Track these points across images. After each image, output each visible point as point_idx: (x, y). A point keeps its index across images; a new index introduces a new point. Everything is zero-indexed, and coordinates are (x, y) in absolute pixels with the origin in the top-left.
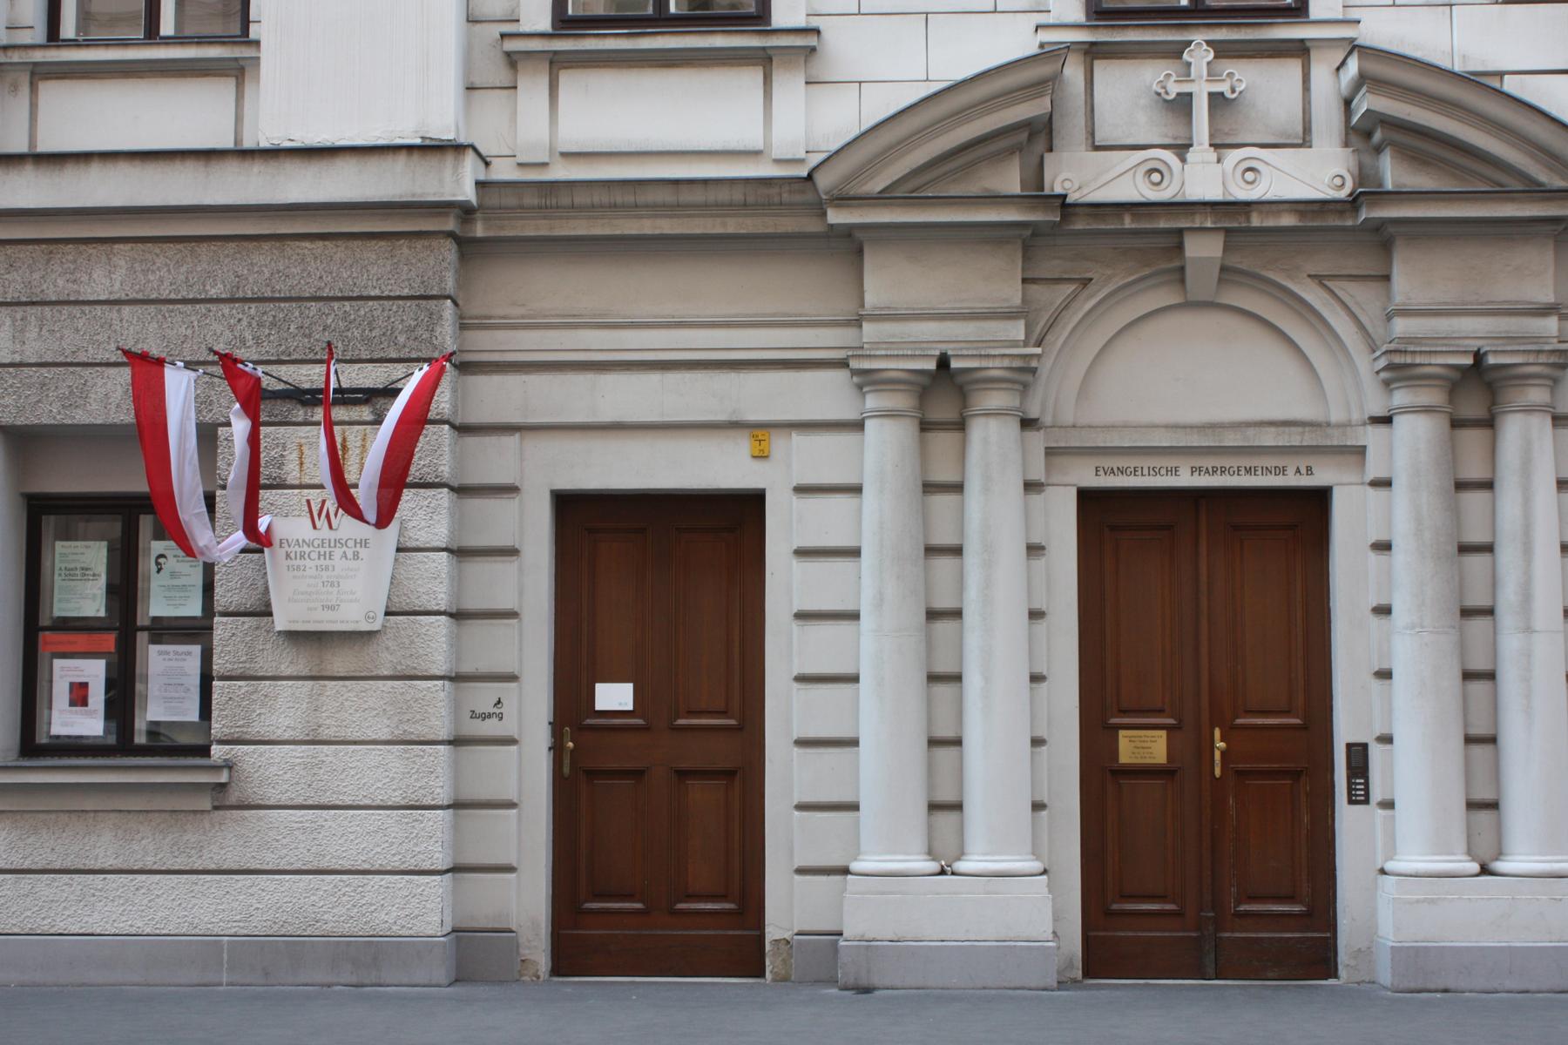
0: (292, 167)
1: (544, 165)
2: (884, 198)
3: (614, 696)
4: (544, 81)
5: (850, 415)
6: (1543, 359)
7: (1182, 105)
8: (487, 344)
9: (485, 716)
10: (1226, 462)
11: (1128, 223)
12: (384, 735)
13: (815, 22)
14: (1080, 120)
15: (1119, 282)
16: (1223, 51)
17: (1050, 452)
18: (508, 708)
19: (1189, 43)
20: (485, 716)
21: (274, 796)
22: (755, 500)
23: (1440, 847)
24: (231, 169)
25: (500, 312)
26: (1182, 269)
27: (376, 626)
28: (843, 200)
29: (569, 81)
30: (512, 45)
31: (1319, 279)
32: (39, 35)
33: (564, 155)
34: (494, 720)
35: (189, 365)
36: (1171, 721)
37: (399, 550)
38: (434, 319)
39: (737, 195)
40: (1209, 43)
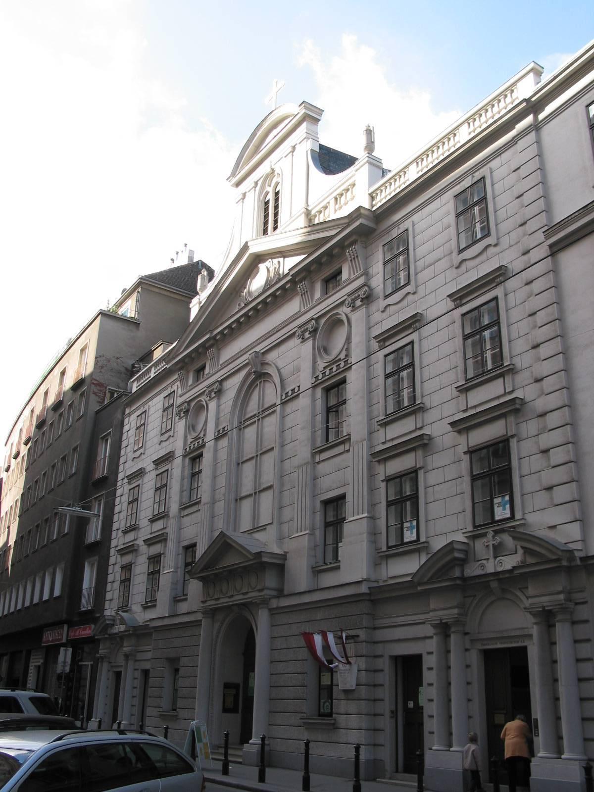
2: (430, 581)
8: (379, 623)
11: (477, 581)
16: (496, 532)
23: (546, 750)
24: (318, 593)
28: (420, 584)
29: (390, 561)
30: (380, 555)
31: (520, 589)
32: (321, 563)
35: (318, 634)
37: (358, 671)
40: (492, 531)
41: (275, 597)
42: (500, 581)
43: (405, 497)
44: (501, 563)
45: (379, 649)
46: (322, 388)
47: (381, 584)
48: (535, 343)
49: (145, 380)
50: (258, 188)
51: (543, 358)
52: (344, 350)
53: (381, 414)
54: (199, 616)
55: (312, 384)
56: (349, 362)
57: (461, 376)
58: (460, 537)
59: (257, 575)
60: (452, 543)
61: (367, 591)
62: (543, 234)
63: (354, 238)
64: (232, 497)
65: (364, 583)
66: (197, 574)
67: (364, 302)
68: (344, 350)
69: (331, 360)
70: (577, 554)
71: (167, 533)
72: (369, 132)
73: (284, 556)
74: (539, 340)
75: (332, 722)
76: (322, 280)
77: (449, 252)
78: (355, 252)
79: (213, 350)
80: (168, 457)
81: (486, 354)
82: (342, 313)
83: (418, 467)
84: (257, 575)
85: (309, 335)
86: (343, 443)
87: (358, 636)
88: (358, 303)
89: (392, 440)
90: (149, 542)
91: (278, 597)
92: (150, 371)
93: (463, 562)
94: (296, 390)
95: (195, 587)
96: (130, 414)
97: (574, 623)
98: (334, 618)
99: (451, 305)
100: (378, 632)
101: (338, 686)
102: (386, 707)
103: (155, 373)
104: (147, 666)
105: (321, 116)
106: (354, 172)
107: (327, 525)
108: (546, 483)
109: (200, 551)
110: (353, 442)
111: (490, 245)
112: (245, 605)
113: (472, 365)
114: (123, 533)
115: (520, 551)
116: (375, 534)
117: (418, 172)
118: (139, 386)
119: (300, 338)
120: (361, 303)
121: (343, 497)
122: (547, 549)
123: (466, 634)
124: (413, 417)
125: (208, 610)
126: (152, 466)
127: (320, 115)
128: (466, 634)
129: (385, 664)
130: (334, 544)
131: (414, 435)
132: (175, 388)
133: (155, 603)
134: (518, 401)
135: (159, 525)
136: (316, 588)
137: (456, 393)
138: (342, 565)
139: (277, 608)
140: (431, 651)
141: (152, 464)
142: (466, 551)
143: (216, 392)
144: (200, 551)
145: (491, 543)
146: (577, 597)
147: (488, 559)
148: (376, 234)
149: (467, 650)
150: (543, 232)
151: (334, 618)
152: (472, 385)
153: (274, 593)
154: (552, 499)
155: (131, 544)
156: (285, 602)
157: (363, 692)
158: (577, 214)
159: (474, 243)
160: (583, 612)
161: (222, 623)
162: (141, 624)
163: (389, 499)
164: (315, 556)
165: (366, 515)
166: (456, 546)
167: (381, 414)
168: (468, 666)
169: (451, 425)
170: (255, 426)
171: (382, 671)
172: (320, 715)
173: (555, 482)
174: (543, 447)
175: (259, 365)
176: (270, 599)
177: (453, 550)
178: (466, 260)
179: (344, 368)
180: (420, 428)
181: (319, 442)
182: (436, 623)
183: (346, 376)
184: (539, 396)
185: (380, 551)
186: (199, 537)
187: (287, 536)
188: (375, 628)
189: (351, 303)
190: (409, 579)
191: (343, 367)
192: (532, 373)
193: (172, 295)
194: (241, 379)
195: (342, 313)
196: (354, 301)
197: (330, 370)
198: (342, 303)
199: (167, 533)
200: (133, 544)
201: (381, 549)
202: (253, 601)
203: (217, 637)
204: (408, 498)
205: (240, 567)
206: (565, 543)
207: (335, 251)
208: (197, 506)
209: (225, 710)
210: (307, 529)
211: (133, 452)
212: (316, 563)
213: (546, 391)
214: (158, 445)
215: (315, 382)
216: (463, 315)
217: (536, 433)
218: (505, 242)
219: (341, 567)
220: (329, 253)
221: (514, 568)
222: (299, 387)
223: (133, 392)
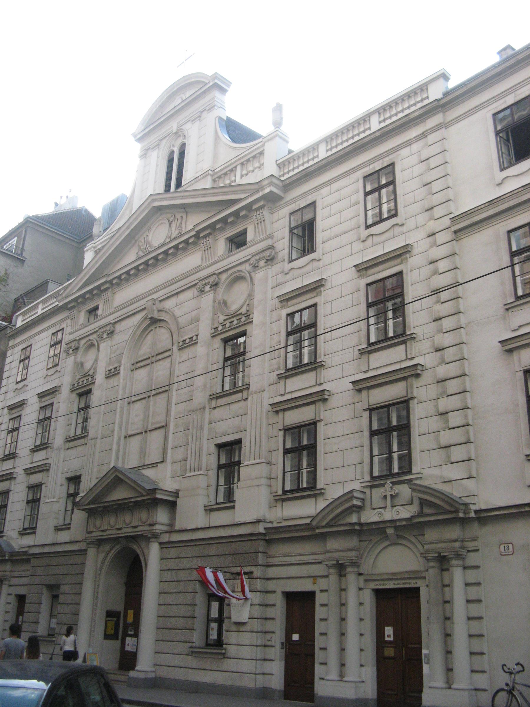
0: (290, 521)
1: (281, 522)
2: (327, 526)
3: (296, 637)
4: (281, 504)
5: (326, 574)
6: (453, 553)
7: (385, 497)
9: (269, 641)
10: (399, 582)
11: (374, 527)
13: (325, 487)
14: (369, 503)
15: (376, 540)
16: (393, 483)
17: (366, 581)
18: (273, 640)
19: (386, 483)
20: (269, 641)
21: (231, 656)
22: (312, 594)
25: (275, 554)
26: (388, 536)
27: (246, 621)
28: (318, 527)
33: (285, 520)
36: (395, 645)
38: (257, 557)
39: (305, 527)
41: (167, 532)
42: (396, 528)
43: (234, 462)
44: (398, 512)
45: (271, 585)
47: (275, 525)
48: (437, 316)
49: (30, 317)
51: (444, 331)
52: (93, 368)
53: (281, 368)
55: (211, 334)
56: (251, 317)
57: (282, 367)
58: (356, 486)
59: (117, 515)
60: (351, 492)
61: (262, 531)
62: (450, 221)
63: (262, 203)
65: (261, 523)
66: (84, 505)
67: (213, 288)
68: (93, 368)
70: (473, 507)
71: (50, 464)
72: (278, 108)
73: (176, 494)
74: (442, 314)
75: (223, 651)
76: (227, 238)
77: (356, 227)
78: (206, 245)
79: (109, 293)
80: (53, 391)
81: (304, 349)
82: (94, 340)
83: (317, 420)
84: (117, 515)
86: (240, 391)
87: (252, 573)
88: (207, 288)
90: (29, 472)
91: (170, 532)
92: (38, 307)
93: (360, 508)
94: (194, 338)
95: (79, 516)
96: (13, 347)
97: (465, 568)
98: (227, 555)
99: (278, 305)
100: (270, 570)
101: (230, 618)
102: (278, 638)
103: (42, 309)
104: (21, 591)
105: (229, 88)
107: (220, 467)
108: (444, 442)
109: (86, 485)
110: (252, 392)
111: (397, 224)
112: (133, 538)
113: (292, 357)
114: (31, 452)
115: (416, 502)
116: (271, 479)
118: (24, 320)
120: (72, 352)
121: (239, 442)
122: (443, 500)
123: (360, 574)
125: (95, 541)
126: (36, 398)
127: (229, 86)
128: (360, 574)
129: (279, 600)
132: (64, 325)
133: (34, 531)
135: (40, 455)
136: (207, 526)
137: (30, 453)
138: (237, 505)
139: (169, 542)
140: (9, 602)
141: (37, 396)
142: (363, 500)
143: (212, 285)
144: (86, 485)
145: (388, 494)
146: (471, 545)
147: (385, 508)
148: (283, 202)
149: (360, 589)
150: (450, 219)
151: (227, 555)
153: (165, 528)
154: (448, 456)
155: (11, 472)
156: (176, 537)
157: (256, 625)
158: (483, 206)
159: (382, 220)
160: (472, 559)
162: (17, 550)
163: (221, 463)
164: (208, 496)
166: (355, 494)
167: (281, 368)
168: (361, 604)
169: (352, 384)
170: (148, 368)
171: (274, 605)
172: (208, 645)
173: (453, 442)
174: (441, 409)
175: (156, 312)
176: (161, 533)
177: (353, 497)
178: (372, 235)
179: (182, 347)
180: (320, 384)
182: (433, 557)
184: (439, 364)
185: (276, 494)
188: (268, 566)
190: (308, 521)
192: (434, 343)
194: (136, 323)
195: (94, 340)
196: (258, 261)
197: (230, 323)
199: (50, 464)
200: (12, 473)
201: (277, 492)
203: (102, 567)
204: (305, 448)
205: (132, 502)
206: (460, 497)
207: (242, 213)
208: (83, 440)
209: (107, 637)
211: (15, 383)
213: (447, 360)
214: (42, 379)
216: (368, 285)
217: (435, 397)
218: (411, 224)
219: (236, 507)
220: (236, 214)
221: (412, 517)
222: (197, 336)
223: (17, 327)
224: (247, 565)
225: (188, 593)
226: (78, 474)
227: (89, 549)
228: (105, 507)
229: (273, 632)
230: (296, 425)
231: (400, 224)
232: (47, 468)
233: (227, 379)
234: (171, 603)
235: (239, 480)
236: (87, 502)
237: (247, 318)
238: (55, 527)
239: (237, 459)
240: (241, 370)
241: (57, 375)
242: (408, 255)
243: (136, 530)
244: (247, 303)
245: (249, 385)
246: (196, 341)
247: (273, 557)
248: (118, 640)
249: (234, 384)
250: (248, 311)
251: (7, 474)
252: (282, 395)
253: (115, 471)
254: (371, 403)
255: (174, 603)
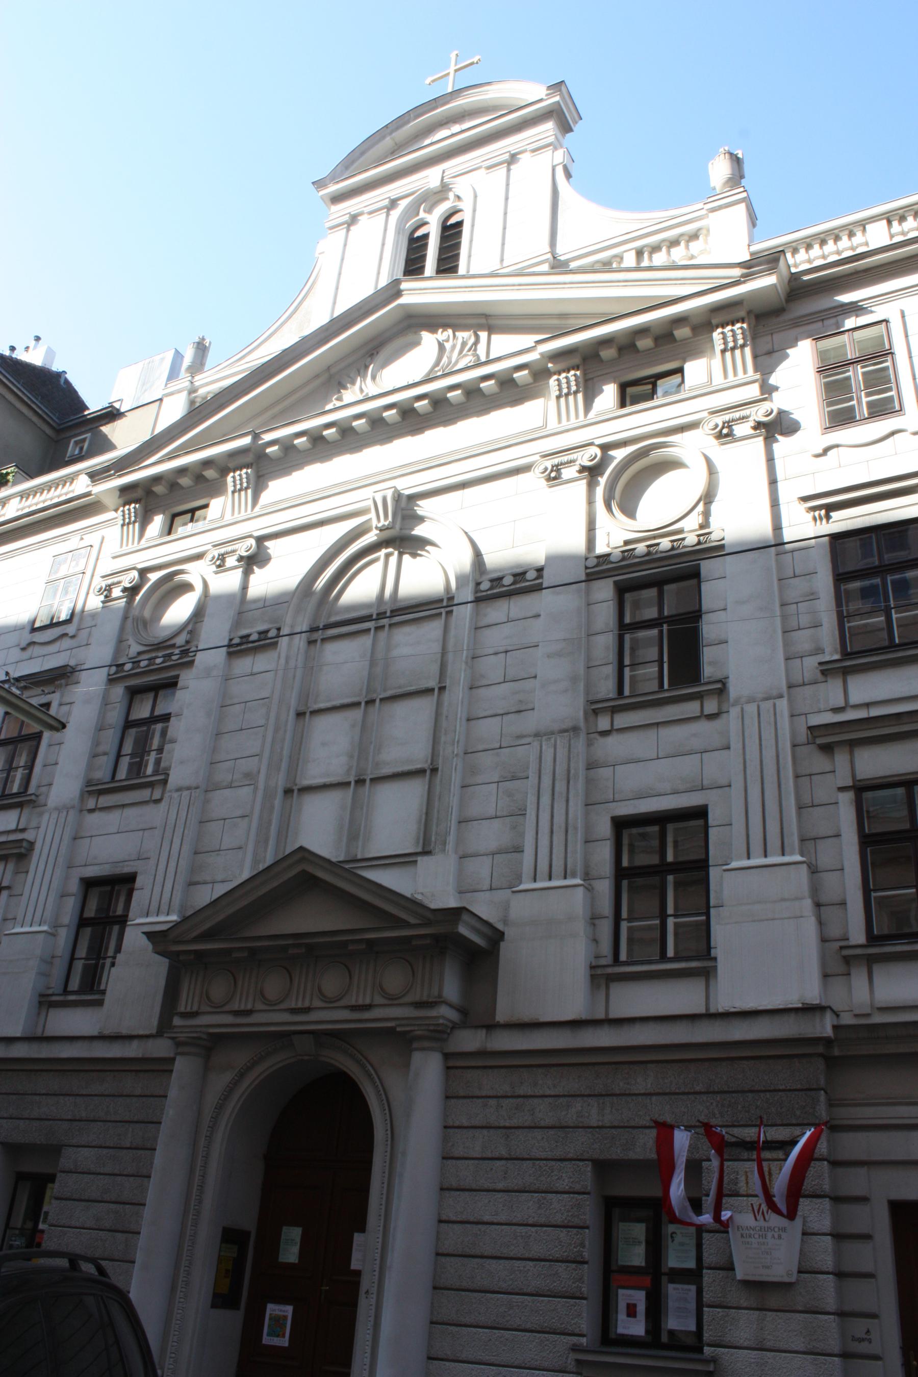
9: (861, 1340)
12: (801, 1347)
20: (861, 1340)
27: (793, 1279)
34: (866, 1344)
35: (688, 1128)
43: (114, 917)
46: (126, 687)
50: (395, 214)
54: (161, 1048)
61: (829, 1032)
64: (280, 782)
69: (156, 643)
85: (121, 594)
86: (151, 785)
89: (867, 705)
106: (703, 212)
107: (83, 922)
117: (18, 510)
119: (102, 594)
121: (129, 880)
124: (18, 810)
125: (204, 1036)
130: (92, 959)
131: (12, 837)
134: (25, 844)
152: (122, 786)
161: (242, 1075)
165: (45, 928)
180: (23, 830)
181: (606, 687)
183: (177, 677)
186: (152, 862)
187: (486, 885)
189: (105, 590)
191: (487, 591)
193: (19, 405)
198: (199, 557)
202: (398, 1029)
210: (45, 922)
212: (597, 957)
215: (115, 674)
224: (779, 1122)
225: (557, 1192)
226: (127, 869)
227: (178, 1058)
228: (253, 951)
229: (874, 1316)
230: (896, 779)
231: (71, 635)
232: (23, 851)
233: (125, 762)
234: (487, 1218)
235: (118, 949)
236: (195, 934)
237: (136, 665)
238: (41, 995)
239: (120, 911)
240: (155, 746)
241: (66, 643)
242: (63, 681)
243: (367, 1015)
244: (190, 627)
245: (168, 775)
246: (276, 640)
247: (856, 1105)
248: (238, 1309)
249: (137, 768)
250: (188, 642)
251: (898, 715)
252: (836, 710)
253: (302, 860)
254: (859, 776)
255: (503, 1218)
